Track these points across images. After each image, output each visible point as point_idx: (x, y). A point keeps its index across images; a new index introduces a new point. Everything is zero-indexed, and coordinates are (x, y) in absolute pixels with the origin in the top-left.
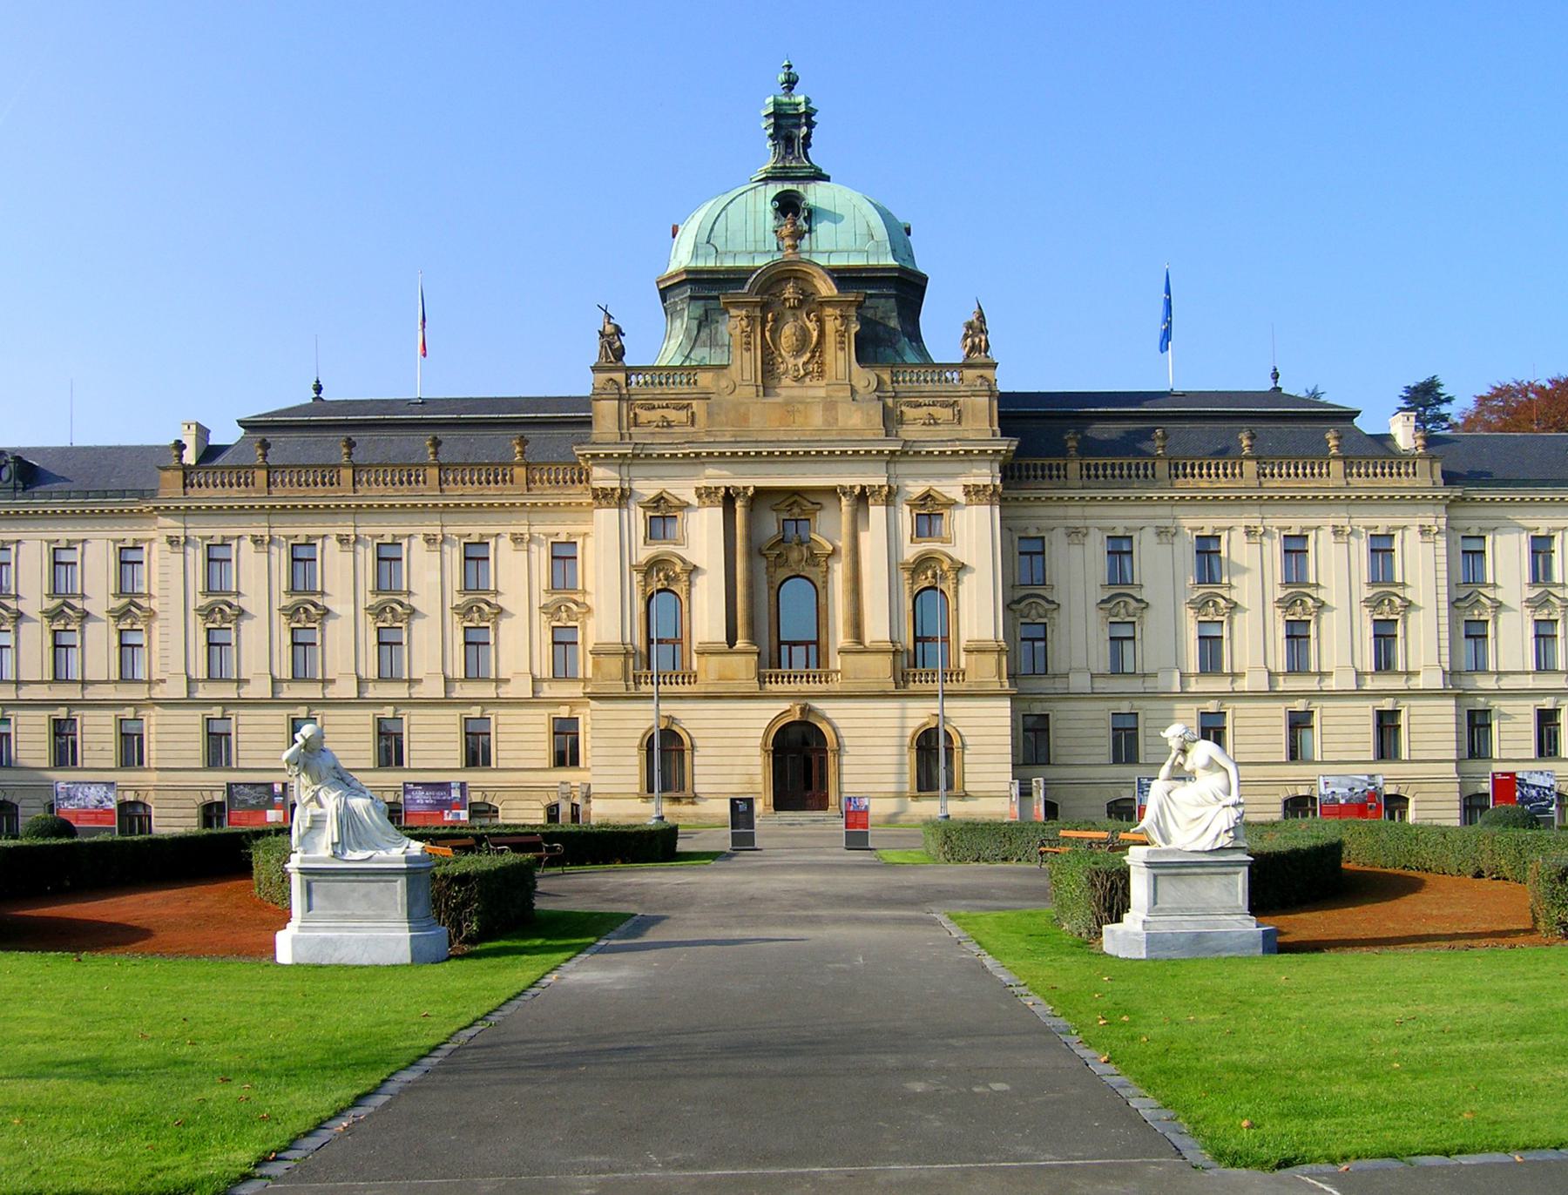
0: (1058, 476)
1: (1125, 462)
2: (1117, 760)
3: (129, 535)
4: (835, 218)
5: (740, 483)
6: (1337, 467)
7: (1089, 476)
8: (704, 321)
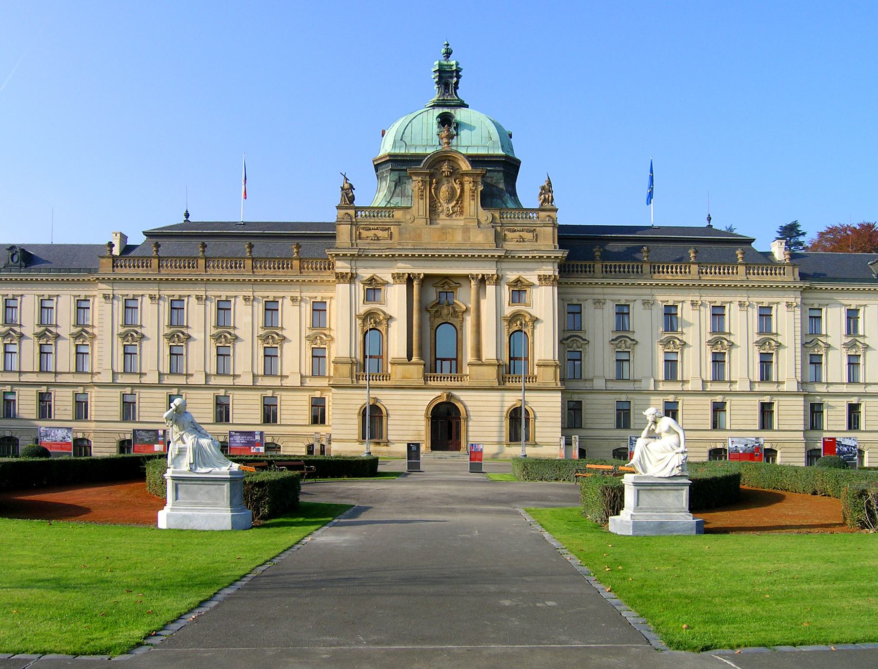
3: (83, 293)
5: (416, 271)
6: (742, 269)
8: (398, 183)
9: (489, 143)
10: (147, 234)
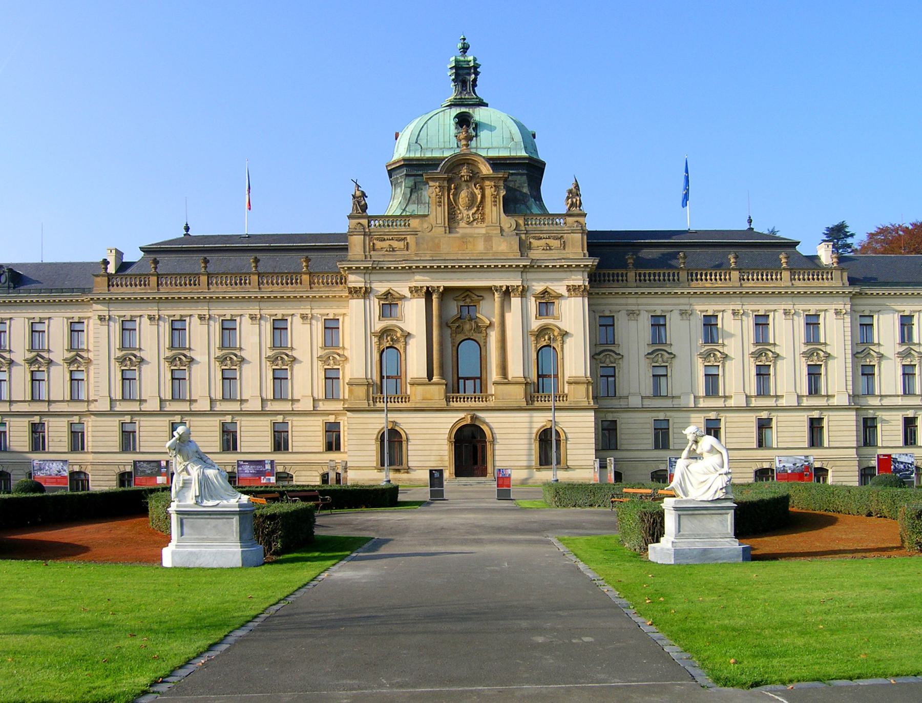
0: (622, 280)
1: (662, 272)
2: (657, 447)
3: (76, 315)
4: (491, 128)
5: (435, 284)
6: (786, 275)
7: (640, 280)
8: (414, 189)
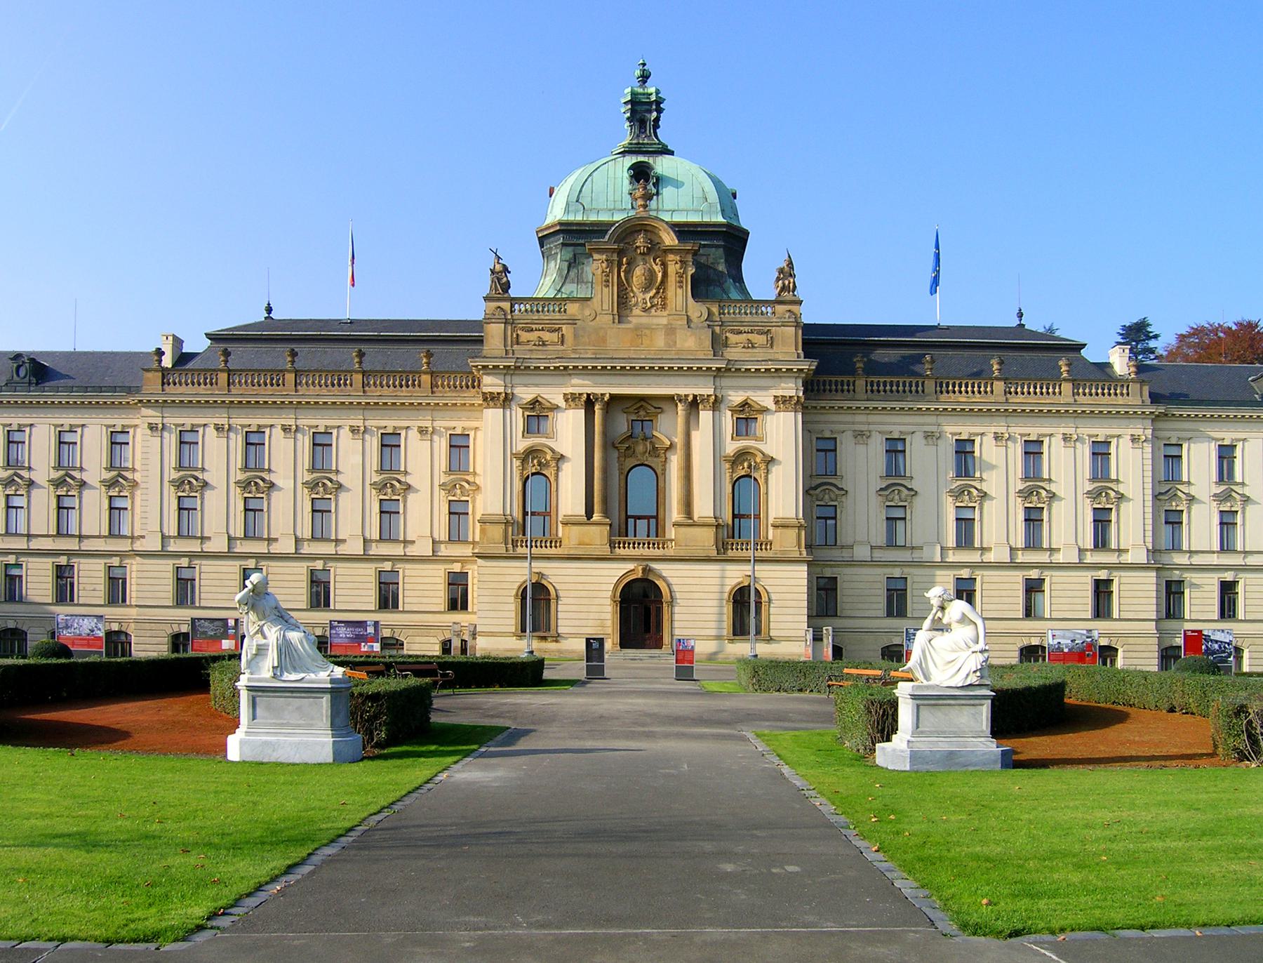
3: (119, 422)
5: (598, 391)
6: (1067, 388)
8: (573, 263)
9: (704, 206)
10: (212, 337)
